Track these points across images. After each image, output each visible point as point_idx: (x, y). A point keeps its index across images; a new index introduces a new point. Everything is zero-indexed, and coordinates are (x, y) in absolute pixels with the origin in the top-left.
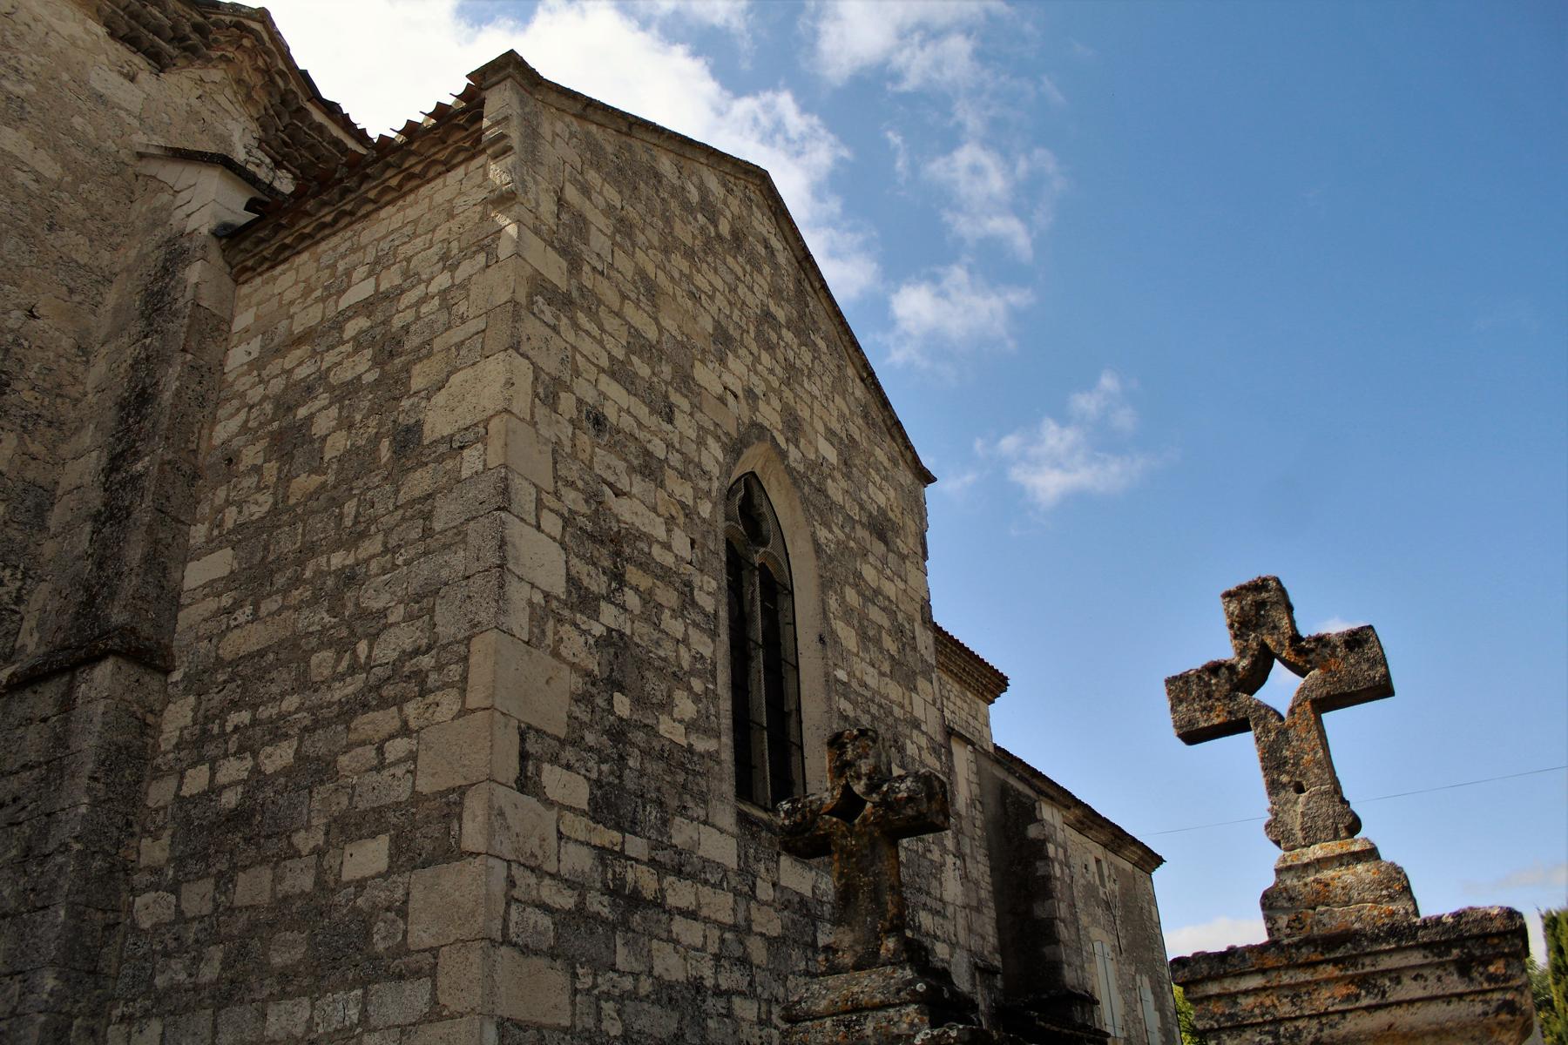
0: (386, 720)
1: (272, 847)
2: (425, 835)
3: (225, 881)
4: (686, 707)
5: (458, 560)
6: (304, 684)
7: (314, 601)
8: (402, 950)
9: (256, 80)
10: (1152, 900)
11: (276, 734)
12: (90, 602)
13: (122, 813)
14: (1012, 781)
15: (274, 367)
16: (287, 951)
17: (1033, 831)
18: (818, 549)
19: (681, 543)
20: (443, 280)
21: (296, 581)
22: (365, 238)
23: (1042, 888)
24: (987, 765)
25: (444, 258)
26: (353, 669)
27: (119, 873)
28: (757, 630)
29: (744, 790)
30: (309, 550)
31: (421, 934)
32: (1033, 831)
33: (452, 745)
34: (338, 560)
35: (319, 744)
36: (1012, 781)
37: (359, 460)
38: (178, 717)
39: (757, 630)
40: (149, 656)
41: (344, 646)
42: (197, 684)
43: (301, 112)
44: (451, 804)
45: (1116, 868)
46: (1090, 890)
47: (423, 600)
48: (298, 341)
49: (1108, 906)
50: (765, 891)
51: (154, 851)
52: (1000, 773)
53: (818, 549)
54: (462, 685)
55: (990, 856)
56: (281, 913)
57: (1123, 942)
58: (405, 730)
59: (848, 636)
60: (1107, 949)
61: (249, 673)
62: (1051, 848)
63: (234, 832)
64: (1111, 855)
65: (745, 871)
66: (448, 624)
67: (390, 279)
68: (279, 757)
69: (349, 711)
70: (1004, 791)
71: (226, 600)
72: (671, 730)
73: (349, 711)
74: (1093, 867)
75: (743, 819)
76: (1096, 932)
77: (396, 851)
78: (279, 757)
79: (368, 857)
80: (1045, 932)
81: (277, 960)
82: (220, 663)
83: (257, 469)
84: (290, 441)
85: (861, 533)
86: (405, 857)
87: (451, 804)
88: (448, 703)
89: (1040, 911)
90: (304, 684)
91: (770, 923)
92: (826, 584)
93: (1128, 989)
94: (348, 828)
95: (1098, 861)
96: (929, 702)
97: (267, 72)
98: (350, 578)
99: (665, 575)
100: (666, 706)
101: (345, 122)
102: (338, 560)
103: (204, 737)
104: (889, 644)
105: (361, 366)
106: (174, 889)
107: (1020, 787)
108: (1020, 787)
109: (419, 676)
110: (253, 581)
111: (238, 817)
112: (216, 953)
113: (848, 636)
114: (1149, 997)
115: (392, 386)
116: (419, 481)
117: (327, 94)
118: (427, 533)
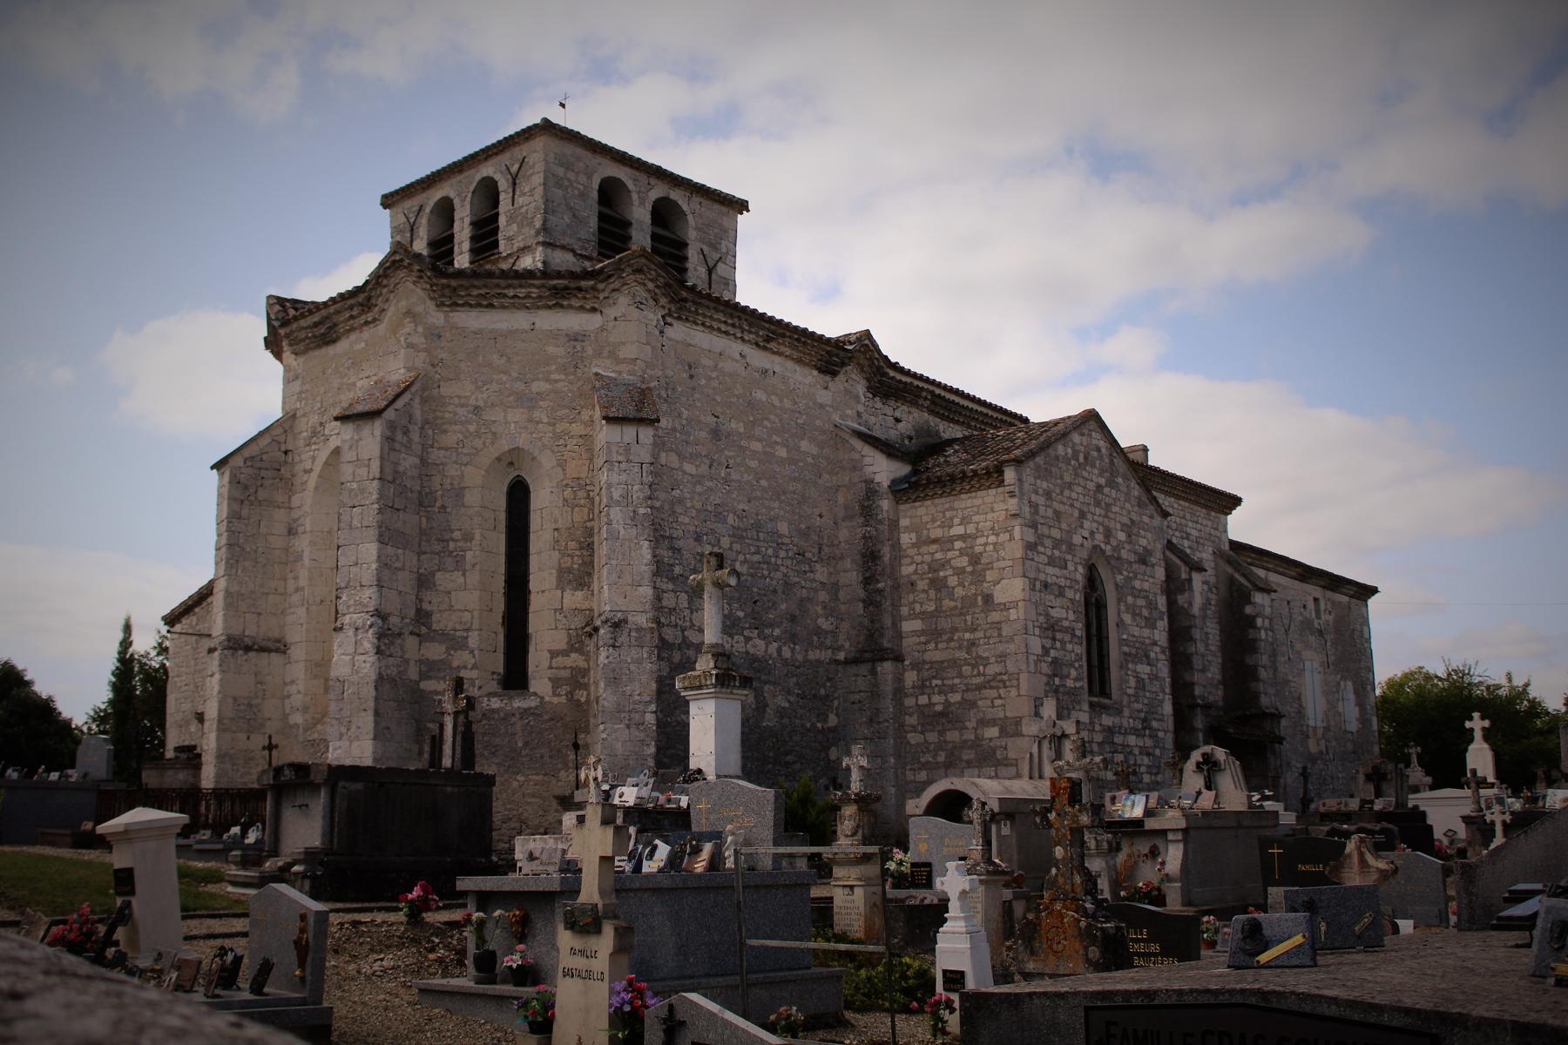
0: (994, 693)
1: (959, 725)
2: (1011, 728)
3: (942, 733)
4: (1073, 673)
5: (1012, 647)
6: (960, 675)
7: (960, 648)
8: (1006, 758)
9: (866, 363)
10: (1366, 622)
11: (953, 689)
12: (871, 635)
13: (901, 710)
14: (1237, 576)
15: (924, 549)
16: (968, 755)
17: (1248, 610)
18: (1117, 585)
19: (1071, 616)
20: (992, 539)
21: (952, 639)
22: (956, 504)
23: (1251, 646)
24: (1222, 563)
25: (992, 529)
26: (979, 674)
27: (901, 729)
28: (1094, 631)
29: (1091, 692)
30: (954, 630)
31: (1011, 755)
32: (1248, 610)
33: (1015, 703)
34: (967, 636)
35: (970, 696)
36: (1237, 576)
37: (969, 602)
38: (910, 677)
39: (1094, 631)
40: (899, 659)
41: (974, 666)
42: (916, 666)
43: (886, 374)
44: (1018, 722)
45: (1333, 603)
46: (1307, 625)
47: (1002, 658)
48: (935, 541)
49: (1321, 633)
50: (1097, 728)
51: (912, 720)
52: (1230, 570)
53: (1117, 585)
54: (1018, 687)
55: (1219, 623)
56: (964, 744)
57: (1332, 658)
58: (1000, 697)
59: (1127, 618)
60: (1316, 665)
61: (939, 668)
62: (1259, 622)
63: (945, 718)
64: (1329, 594)
65: (1092, 723)
66: (1011, 668)
67: (971, 529)
68: (955, 698)
69: (979, 688)
70: (1232, 581)
71: (923, 639)
72: (1070, 683)
73: (979, 688)
74: (1311, 605)
75: (1091, 705)
76: (1307, 654)
77: (1001, 731)
78: (955, 698)
79: (993, 732)
80: (1251, 673)
81: (965, 757)
82: (924, 662)
83: (924, 591)
84: (938, 585)
85: (1135, 566)
86: (1004, 733)
87: (1018, 722)
88: (1014, 692)
89: (1250, 661)
90: (960, 675)
91: (1099, 738)
92: (1119, 600)
93: (1332, 693)
94: (984, 723)
95: (1316, 600)
96: (1188, 522)
97: (871, 359)
98: (973, 644)
99: (1066, 630)
100: (1068, 676)
101: (902, 370)
102: (967, 636)
103: (923, 686)
104: (1145, 612)
105: (963, 562)
106: (922, 733)
107: (1242, 580)
108: (1242, 580)
109: (1003, 681)
110: (934, 634)
111: (942, 714)
112: (943, 754)
113: (1127, 618)
114: (1351, 696)
115: (979, 577)
116: (995, 616)
117: (893, 360)
118: (1000, 635)
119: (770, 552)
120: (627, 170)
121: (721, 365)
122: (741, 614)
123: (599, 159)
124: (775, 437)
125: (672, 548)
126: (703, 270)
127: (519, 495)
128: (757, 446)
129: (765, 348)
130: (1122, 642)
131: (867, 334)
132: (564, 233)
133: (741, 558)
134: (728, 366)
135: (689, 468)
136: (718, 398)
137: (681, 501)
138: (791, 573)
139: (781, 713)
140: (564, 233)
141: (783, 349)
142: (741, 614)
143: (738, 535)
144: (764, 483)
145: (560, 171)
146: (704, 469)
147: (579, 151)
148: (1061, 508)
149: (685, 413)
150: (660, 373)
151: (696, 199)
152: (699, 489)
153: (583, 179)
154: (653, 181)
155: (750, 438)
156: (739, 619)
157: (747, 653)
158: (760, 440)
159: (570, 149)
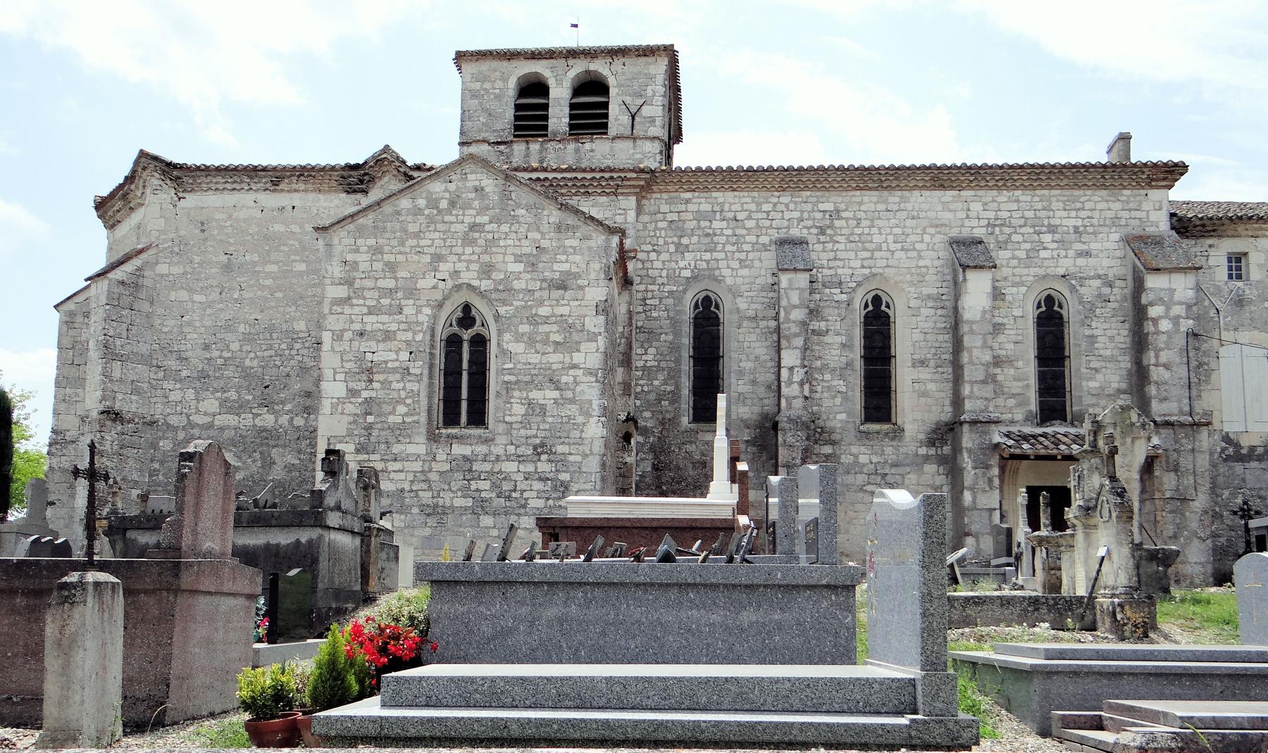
119: (284, 346)
120: (544, 62)
121: (235, 215)
122: (250, 397)
123: (514, 63)
124: (292, 257)
125: (180, 359)
126: (626, 119)
127: (878, 324)
128: (273, 268)
129: (274, 191)
130: (502, 371)
131: (387, 148)
132: (480, 131)
133: (252, 355)
134: (242, 214)
135: (197, 298)
136: (232, 241)
137: (189, 324)
138: (306, 359)
139: (289, 468)
140: (480, 131)
141: (294, 186)
142: (250, 397)
143: (247, 338)
144: (279, 295)
145: (477, 86)
146: (214, 296)
147: (495, 64)
148: (391, 258)
149: (197, 259)
150: (172, 236)
151: (618, 63)
152: (209, 311)
153: (499, 84)
154: (571, 62)
155: (265, 263)
156: (248, 401)
157: (254, 426)
158: (276, 263)
159: (485, 66)
